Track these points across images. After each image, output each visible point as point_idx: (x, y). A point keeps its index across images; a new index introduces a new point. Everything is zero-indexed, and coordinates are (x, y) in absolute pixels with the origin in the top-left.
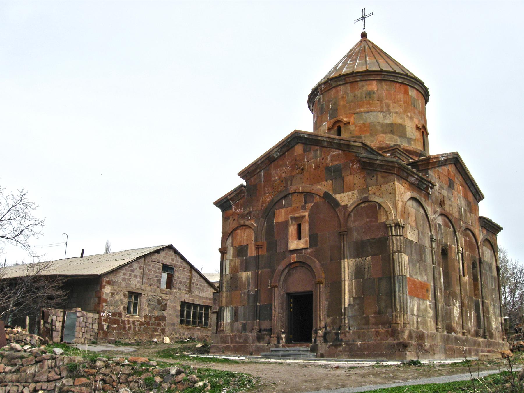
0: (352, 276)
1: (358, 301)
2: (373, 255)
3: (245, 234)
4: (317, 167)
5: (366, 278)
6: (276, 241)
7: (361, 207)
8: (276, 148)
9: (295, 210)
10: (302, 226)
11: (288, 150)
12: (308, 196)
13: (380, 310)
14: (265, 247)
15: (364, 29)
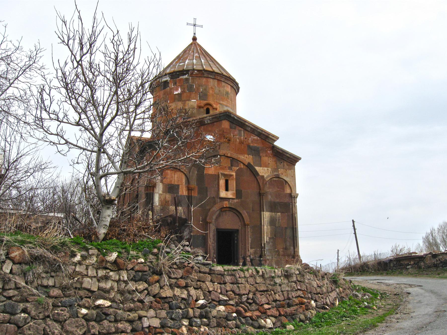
0: (268, 223)
1: (272, 240)
2: (282, 213)
3: (176, 176)
4: (241, 143)
5: (277, 226)
6: (207, 188)
7: (274, 180)
8: (252, 125)
9: (223, 168)
10: (229, 182)
11: (216, 122)
12: (234, 161)
13: (286, 247)
14: (197, 191)
15: (195, 34)
